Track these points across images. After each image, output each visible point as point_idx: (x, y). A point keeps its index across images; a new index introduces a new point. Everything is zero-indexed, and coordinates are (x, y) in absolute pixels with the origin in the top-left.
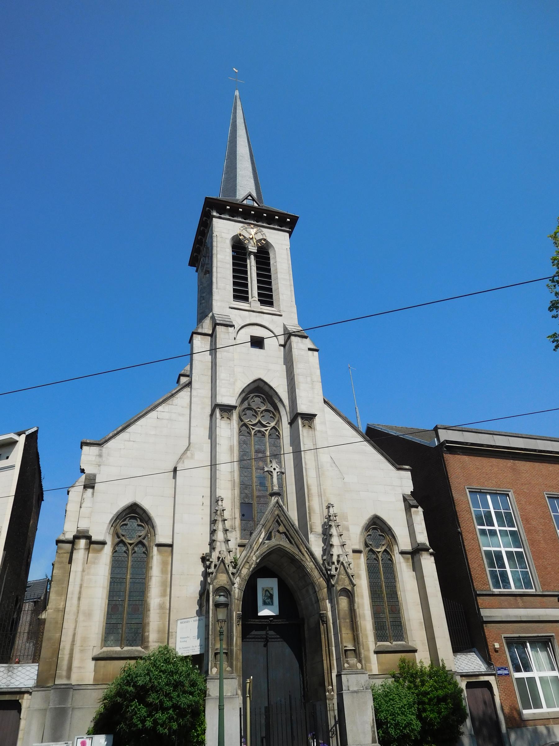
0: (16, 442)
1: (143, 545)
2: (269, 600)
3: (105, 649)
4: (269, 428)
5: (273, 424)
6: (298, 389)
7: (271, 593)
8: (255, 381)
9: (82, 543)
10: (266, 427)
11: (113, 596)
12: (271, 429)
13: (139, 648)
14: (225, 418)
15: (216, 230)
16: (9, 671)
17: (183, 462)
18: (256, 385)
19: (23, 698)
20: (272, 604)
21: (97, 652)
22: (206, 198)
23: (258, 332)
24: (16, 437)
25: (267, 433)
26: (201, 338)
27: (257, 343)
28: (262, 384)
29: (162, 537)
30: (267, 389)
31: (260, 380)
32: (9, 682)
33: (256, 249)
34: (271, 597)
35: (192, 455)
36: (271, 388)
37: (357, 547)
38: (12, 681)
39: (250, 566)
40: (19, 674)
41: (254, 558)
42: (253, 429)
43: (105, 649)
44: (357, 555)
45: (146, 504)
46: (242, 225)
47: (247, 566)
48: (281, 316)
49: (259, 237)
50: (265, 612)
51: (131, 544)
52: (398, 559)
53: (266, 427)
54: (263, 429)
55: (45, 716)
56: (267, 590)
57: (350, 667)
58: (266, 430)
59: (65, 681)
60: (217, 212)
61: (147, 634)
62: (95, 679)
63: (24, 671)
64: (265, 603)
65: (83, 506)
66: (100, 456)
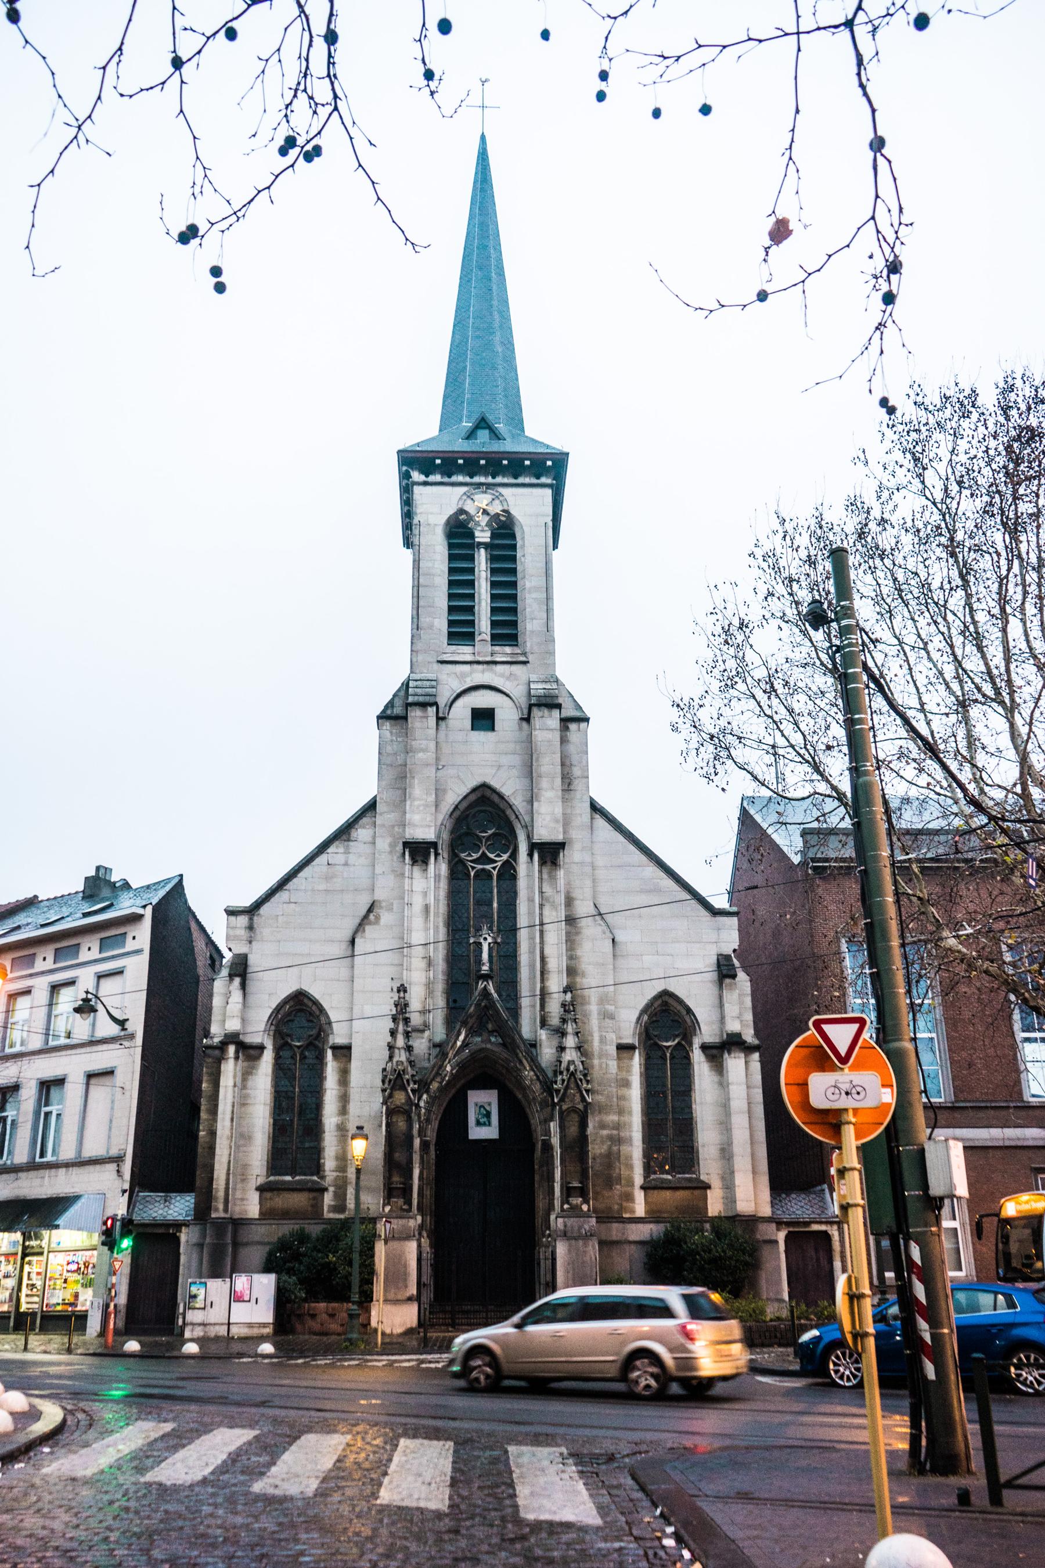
0: (141, 916)
1: (316, 1047)
2: (485, 1119)
3: (272, 1178)
4: (499, 864)
5: (505, 857)
6: (537, 800)
7: (488, 1108)
8: (474, 790)
9: (232, 1049)
10: (496, 862)
11: (279, 1115)
12: (502, 865)
13: (315, 1178)
14: (420, 863)
15: (418, 511)
16: (166, 1201)
17: (364, 931)
18: (478, 794)
19: (181, 1232)
20: (490, 1125)
21: (261, 1180)
22: (399, 452)
23: (483, 700)
24: (141, 911)
25: (495, 873)
26: (391, 726)
27: (483, 719)
28: (488, 793)
29: (338, 1038)
30: (496, 799)
31: (484, 786)
32: (631, 1505)
33: (488, 534)
34: (488, 1115)
35: (378, 918)
36: (501, 796)
37: (628, 1040)
38: (171, 1212)
39: (443, 1079)
40: (177, 1204)
41: (448, 1068)
42: (473, 868)
43: (272, 1178)
44: (625, 1054)
45: (316, 991)
46: (464, 489)
47: (439, 1079)
48: (525, 663)
49: (496, 508)
50: (477, 1133)
51: (299, 1047)
52: (697, 1056)
53: (496, 862)
54: (488, 867)
55: (203, 1249)
56: (481, 1106)
57: (571, 1208)
58: (494, 868)
59: (222, 1215)
60: (422, 472)
61: (322, 1161)
62: (261, 1213)
63: (183, 1201)
64: (478, 1123)
65: (230, 1001)
66: (251, 928)
